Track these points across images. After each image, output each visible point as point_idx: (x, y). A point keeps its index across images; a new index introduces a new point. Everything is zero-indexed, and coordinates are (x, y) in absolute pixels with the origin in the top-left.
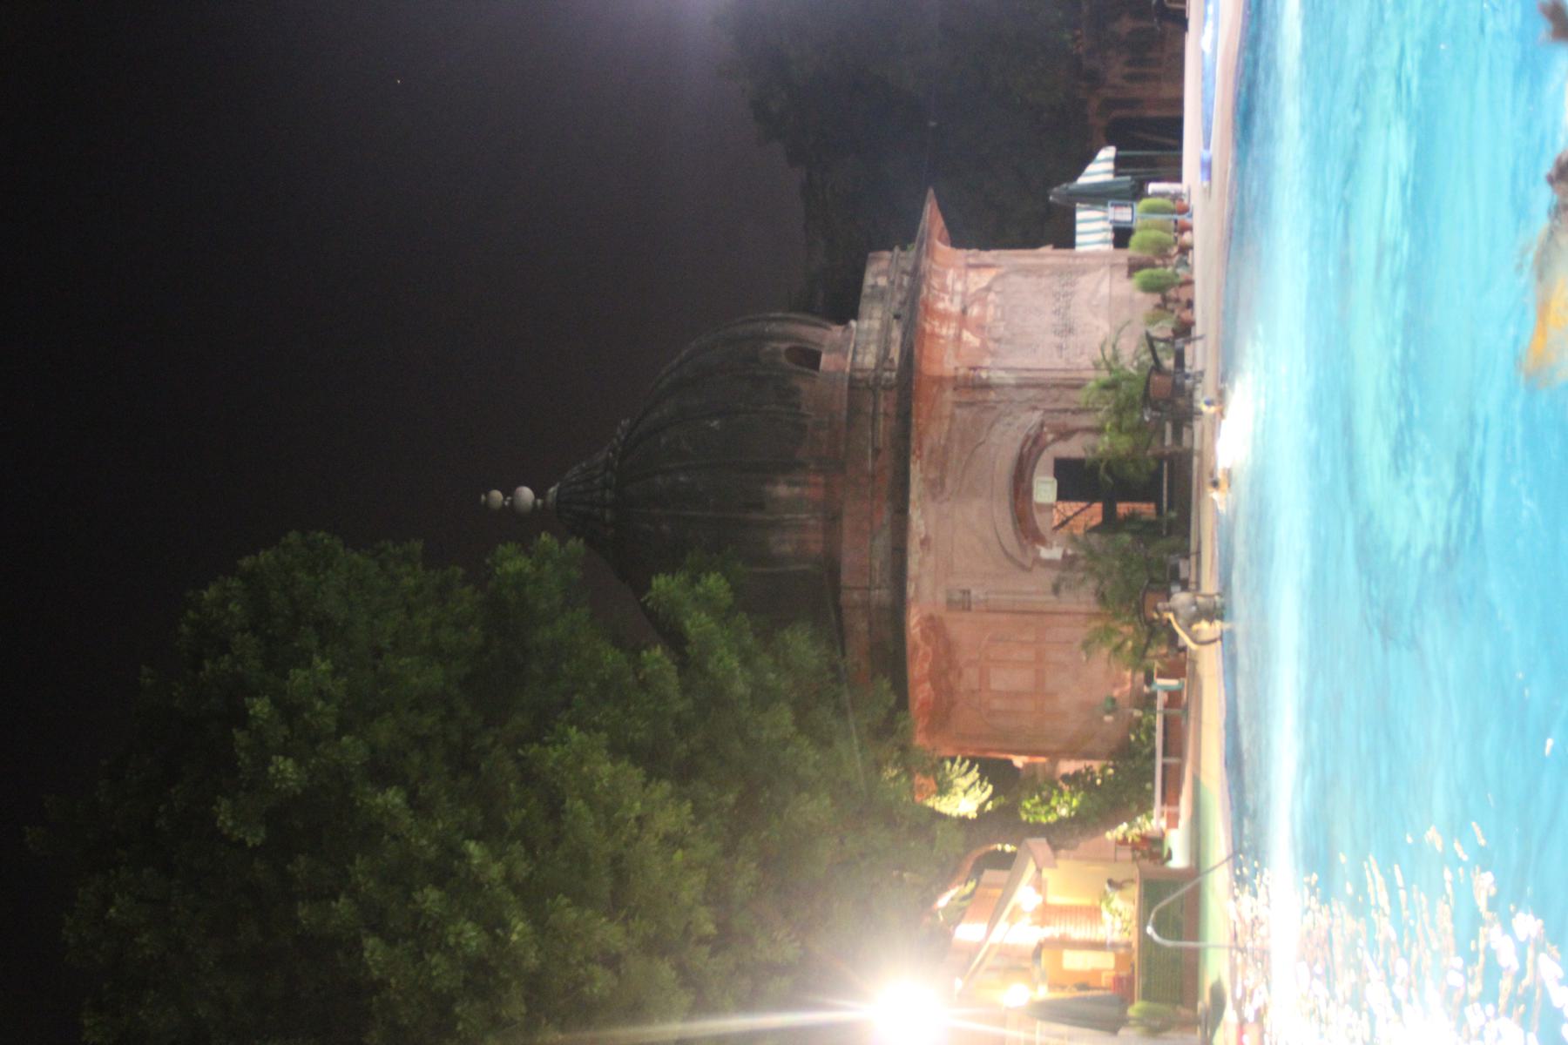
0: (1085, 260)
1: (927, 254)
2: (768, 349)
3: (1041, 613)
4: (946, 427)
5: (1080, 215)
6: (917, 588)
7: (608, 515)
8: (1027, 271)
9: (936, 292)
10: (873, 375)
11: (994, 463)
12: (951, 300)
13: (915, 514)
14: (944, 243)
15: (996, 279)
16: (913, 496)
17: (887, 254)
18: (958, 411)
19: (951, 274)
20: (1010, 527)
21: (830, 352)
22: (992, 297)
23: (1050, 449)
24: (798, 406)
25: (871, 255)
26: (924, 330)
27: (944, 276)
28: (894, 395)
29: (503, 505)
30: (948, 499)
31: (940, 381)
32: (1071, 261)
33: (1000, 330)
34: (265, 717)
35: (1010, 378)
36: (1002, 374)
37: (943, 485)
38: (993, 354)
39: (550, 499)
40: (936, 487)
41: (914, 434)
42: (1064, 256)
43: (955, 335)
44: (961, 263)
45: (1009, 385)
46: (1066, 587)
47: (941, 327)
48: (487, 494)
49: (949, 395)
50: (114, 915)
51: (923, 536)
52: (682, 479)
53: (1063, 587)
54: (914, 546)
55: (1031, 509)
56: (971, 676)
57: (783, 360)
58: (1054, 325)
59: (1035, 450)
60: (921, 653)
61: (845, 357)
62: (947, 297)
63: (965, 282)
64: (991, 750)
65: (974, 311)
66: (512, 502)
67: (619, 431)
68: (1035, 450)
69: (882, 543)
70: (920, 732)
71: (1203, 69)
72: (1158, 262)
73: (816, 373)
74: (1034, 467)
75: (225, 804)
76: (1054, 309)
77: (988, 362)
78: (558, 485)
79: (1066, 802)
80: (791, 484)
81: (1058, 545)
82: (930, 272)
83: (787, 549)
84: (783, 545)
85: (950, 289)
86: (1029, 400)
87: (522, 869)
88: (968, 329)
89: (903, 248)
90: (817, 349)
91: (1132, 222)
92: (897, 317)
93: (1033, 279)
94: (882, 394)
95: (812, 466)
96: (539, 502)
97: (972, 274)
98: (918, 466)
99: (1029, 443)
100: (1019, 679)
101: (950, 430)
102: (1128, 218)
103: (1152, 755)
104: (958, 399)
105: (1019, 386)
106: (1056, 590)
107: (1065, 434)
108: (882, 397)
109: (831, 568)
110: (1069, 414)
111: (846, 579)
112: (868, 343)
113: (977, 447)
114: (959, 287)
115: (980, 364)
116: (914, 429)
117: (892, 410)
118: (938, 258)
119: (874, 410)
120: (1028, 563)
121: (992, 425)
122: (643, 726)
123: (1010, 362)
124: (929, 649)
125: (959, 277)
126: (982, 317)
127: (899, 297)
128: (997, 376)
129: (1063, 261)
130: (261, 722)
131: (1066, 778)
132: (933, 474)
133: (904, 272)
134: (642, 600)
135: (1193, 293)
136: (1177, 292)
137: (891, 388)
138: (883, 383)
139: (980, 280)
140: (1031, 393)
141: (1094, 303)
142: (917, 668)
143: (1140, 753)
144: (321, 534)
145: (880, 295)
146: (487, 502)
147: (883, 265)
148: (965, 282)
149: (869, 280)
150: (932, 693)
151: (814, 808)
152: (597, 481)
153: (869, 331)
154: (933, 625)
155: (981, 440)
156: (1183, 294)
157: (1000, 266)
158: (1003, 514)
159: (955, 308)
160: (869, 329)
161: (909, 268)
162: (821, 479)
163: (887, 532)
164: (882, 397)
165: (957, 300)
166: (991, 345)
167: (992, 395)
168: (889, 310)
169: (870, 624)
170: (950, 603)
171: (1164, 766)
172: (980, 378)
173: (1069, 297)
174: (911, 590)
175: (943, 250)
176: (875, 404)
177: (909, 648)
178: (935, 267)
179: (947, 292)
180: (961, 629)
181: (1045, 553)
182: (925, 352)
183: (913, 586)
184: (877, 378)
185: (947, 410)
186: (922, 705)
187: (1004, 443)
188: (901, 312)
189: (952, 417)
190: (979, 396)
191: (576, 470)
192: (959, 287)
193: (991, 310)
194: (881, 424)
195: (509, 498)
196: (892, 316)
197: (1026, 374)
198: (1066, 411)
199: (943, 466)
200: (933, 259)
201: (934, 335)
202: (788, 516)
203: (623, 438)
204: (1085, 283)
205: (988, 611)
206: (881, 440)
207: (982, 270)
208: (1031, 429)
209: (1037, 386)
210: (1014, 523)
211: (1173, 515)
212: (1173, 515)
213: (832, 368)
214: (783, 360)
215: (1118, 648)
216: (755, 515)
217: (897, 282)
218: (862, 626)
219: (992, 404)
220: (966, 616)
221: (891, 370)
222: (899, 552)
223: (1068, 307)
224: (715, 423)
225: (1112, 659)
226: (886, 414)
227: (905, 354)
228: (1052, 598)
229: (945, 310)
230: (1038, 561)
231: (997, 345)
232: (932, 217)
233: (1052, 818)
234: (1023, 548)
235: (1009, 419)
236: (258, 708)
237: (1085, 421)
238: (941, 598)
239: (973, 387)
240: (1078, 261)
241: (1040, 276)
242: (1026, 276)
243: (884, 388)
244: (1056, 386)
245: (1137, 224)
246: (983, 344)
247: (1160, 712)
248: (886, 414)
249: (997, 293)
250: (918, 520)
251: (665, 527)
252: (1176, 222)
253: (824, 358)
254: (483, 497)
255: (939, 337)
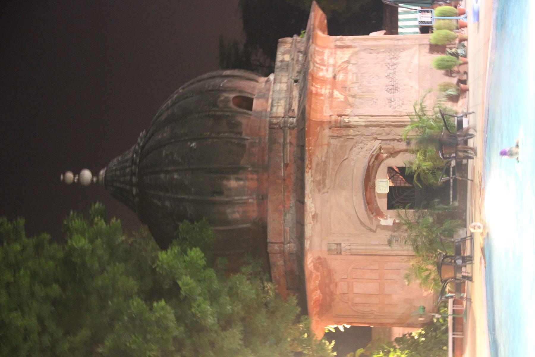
0: (404, 42)
1: (313, 42)
2: (222, 98)
4: (326, 150)
5: (400, 10)
6: (310, 244)
7: (135, 191)
8: (370, 49)
11: (353, 171)
12: (327, 70)
13: (308, 201)
14: (324, 32)
15: (352, 55)
16: (307, 191)
17: (289, 39)
18: (332, 141)
19: (327, 52)
20: (363, 207)
22: (350, 67)
23: (385, 162)
24: (241, 133)
25: (280, 40)
26: (311, 92)
27: (322, 53)
28: (295, 132)
29: (74, 181)
30: (327, 192)
31: (321, 123)
32: (396, 42)
33: (355, 90)
35: (361, 121)
36: (356, 119)
37: (324, 184)
38: (352, 106)
39: (101, 178)
42: (391, 39)
43: (329, 93)
44: (332, 45)
45: (361, 126)
47: (321, 89)
48: (64, 174)
49: (327, 132)
51: (313, 214)
52: (176, 176)
54: (308, 219)
56: (342, 287)
57: (231, 104)
59: (376, 163)
60: (314, 276)
61: (267, 101)
65: (341, 77)
66: (78, 179)
67: (139, 140)
68: (376, 163)
69: (290, 217)
73: (250, 112)
76: (386, 75)
77: (348, 111)
78: (105, 169)
80: (238, 179)
81: (390, 218)
83: (237, 216)
85: (326, 63)
86: (372, 134)
88: (337, 90)
89: (299, 34)
90: (249, 96)
92: (296, 81)
93: (374, 55)
94: (288, 131)
96: (95, 179)
97: (339, 52)
98: (310, 174)
99: (373, 159)
100: (372, 287)
101: (327, 152)
102: (429, 20)
103: (446, 331)
104: (331, 134)
105: (366, 126)
106: (390, 243)
107: (393, 154)
108: (288, 134)
111: (271, 237)
112: (279, 99)
114: (331, 61)
115: (344, 113)
116: (307, 142)
117: (294, 141)
118: (319, 42)
119: (284, 142)
120: (374, 228)
121: (351, 149)
123: (361, 111)
126: (345, 81)
127: (297, 68)
128: (353, 120)
129: (391, 42)
131: (398, 340)
135: (468, 68)
136: (458, 68)
137: (293, 128)
139: (343, 55)
140: (374, 129)
142: (312, 283)
145: (287, 66)
147: (287, 47)
149: (279, 57)
150: (321, 295)
152: (128, 170)
153: (280, 91)
154: (320, 262)
155: (346, 157)
156: (462, 69)
157: (355, 47)
158: (358, 199)
159: (329, 75)
160: (279, 90)
161: (302, 49)
162: (255, 176)
163: (293, 211)
164: (288, 134)
165: (331, 69)
166: (350, 99)
167: (351, 132)
168: (291, 78)
169: (285, 261)
172: (345, 122)
175: (322, 36)
176: (285, 139)
177: (307, 273)
179: (324, 65)
181: (383, 222)
182: (313, 106)
183: (309, 242)
186: (315, 302)
189: (329, 145)
191: (115, 161)
192: (331, 61)
193: (350, 77)
194: (288, 148)
196: (293, 81)
198: (394, 140)
199: (324, 174)
200: (316, 44)
202: (236, 198)
203: (141, 144)
204: (404, 56)
205: (352, 255)
206: (288, 159)
207: (344, 49)
212: (456, 204)
213: (259, 109)
214: (231, 104)
216: (218, 198)
217: (295, 60)
218: (280, 262)
220: (338, 257)
222: (300, 224)
224: (194, 144)
225: (423, 285)
226: (291, 143)
228: (388, 248)
229: (323, 77)
230: (379, 226)
231: (354, 99)
234: (370, 219)
235: (361, 145)
238: (325, 248)
243: (289, 128)
245: (434, 24)
246: (346, 99)
248: (291, 143)
250: (310, 205)
251: (167, 203)
252: (457, 20)
253: (255, 102)
254: (62, 177)
255: (322, 95)
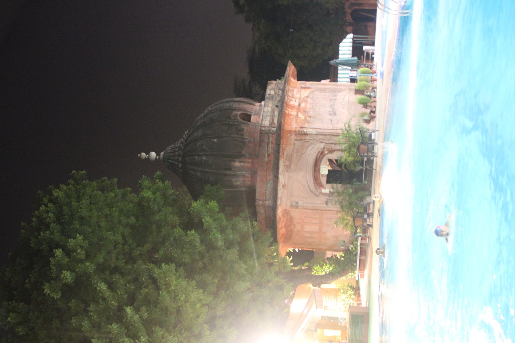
0: (341, 87)
1: (288, 84)
2: (234, 114)
3: (321, 210)
4: (292, 148)
8: (321, 90)
9: (290, 98)
10: (268, 129)
12: (295, 101)
13: (281, 177)
14: (294, 79)
15: (310, 93)
16: (280, 171)
17: (274, 82)
18: (296, 142)
19: (296, 91)
20: (312, 182)
21: (254, 115)
22: (309, 100)
24: (243, 135)
25: (269, 82)
26: (286, 113)
27: (293, 91)
28: (275, 136)
29: (146, 158)
30: (292, 172)
31: (290, 132)
32: (336, 87)
34: (60, 257)
35: (314, 132)
36: (311, 130)
37: (290, 167)
38: (309, 122)
40: (288, 167)
41: (281, 150)
42: (333, 85)
43: (296, 114)
44: (299, 86)
45: (313, 134)
46: (330, 202)
47: (291, 111)
48: (140, 154)
49: (293, 137)
50: (10, 320)
51: (283, 184)
53: (329, 202)
54: (280, 187)
55: (319, 176)
56: (298, 227)
57: (239, 118)
58: (329, 112)
59: (321, 156)
60: (282, 220)
62: (294, 100)
63: (300, 94)
64: (304, 248)
65: (303, 105)
67: (184, 136)
69: (270, 185)
70: (281, 242)
71: (382, 32)
72: (354, 202)
73: (249, 123)
74: (321, 160)
75: (47, 285)
76: (329, 105)
78: (164, 151)
79: (328, 268)
80: (241, 162)
81: (328, 188)
82: (288, 91)
84: (238, 182)
86: (320, 139)
87: (145, 315)
88: (300, 112)
91: (356, 77)
92: (277, 106)
94: (271, 135)
95: (247, 156)
98: (282, 161)
99: (319, 154)
100: (315, 228)
102: (356, 75)
103: (356, 254)
104: (297, 138)
105: (317, 135)
106: (327, 203)
107: (331, 151)
109: (251, 192)
110: (333, 144)
111: (257, 197)
112: (267, 116)
113: (302, 155)
114: (298, 96)
117: (274, 142)
118: (292, 84)
119: (268, 142)
120: (318, 194)
121: (307, 147)
122: (188, 257)
123: (314, 126)
124: (285, 219)
125: (298, 91)
126: (305, 108)
127: (278, 99)
128: (309, 131)
130: (58, 258)
131: (328, 259)
132: (287, 163)
133: (280, 89)
134: (189, 210)
135: (376, 104)
137: (274, 134)
138: (271, 132)
139: (305, 93)
140: (321, 137)
141: (343, 103)
142: (281, 224)
143: (353, 253)
144: (60, 295)
145: (272, 97)
146: (140, 156)
148: (300, 94)
149: (268, 92)
151: (242, 286)
152: (177, 153)
153: (267, 112)
154: (286, 213)
155: (304, 152)
157: (312, 88)
159: (296, 104)
160: (267, 111)
161: (282, 88)
162: (250, 161)
165: (297, 100)
166: (308, 119)
167: (308, 137)
169: (265, 211)
170: (292, 206)
171: (360, 259)
173: (335, 101)
174: (279, 202)
175: (293, 81)
176: (269, 140)
178: (290, 88)
179: (294, 98)
180: (295, 213)
181: (323, 191)
182: (286, 121)
183: (280, 201)
184: (269, 130)
185: (292, 142)
186: (282, 235)
187: (311, 153)
188: (278, 105)
189: (294, 144)
190: (303, 137)
192: (298, 96)
194: (270, 145)
195: (148, 155)
196: (275, 106)
197: (320, 131)
198: (332, 143)
199: (291, 161)
200: (290, 86)
201: (289, 115)
202: (239, 173)
204: (340, 95)
205: (304, 209)
207: (306, 89)
208: (320, 150)
209: (321, 135)
210: (313, 180)
211: (366, 182)
213: (255, 121)
215: (347, 224)
216: (228, 172)
218: (263, 211)
219: (307, 140)
220: (297, 210)
221: (274, 127)
222: (275, 190)
223: (334, 105)
225: (344, 229)
226: (272, 142)
227: (279, 124)
228: (325, 206)
229: (293, 105)
232: (291, 69)
233: (324, 273)
234: (316, 189)
236: (58, 253)
237: (337, 147)
238: (289, 204)
239: (302, 134)
240: (338, 87)
241: (325, 92)
242: (321, 92)
243: (272, 134)
244: (329, 135)
245: (358, 78)
246: (305, 118)
247: (359, 246)
249: (311, 98)
250: (282, 179)
253: (252, 117)
254: (139, 155)
255: (291, 115)
